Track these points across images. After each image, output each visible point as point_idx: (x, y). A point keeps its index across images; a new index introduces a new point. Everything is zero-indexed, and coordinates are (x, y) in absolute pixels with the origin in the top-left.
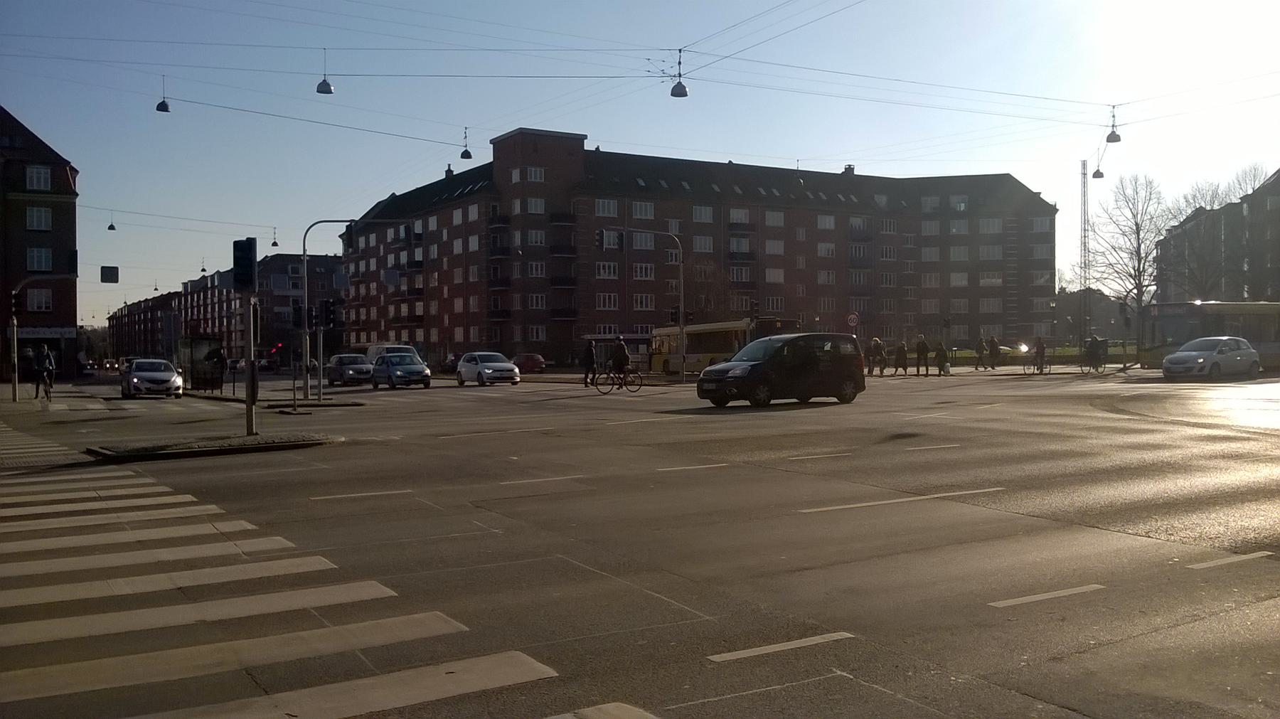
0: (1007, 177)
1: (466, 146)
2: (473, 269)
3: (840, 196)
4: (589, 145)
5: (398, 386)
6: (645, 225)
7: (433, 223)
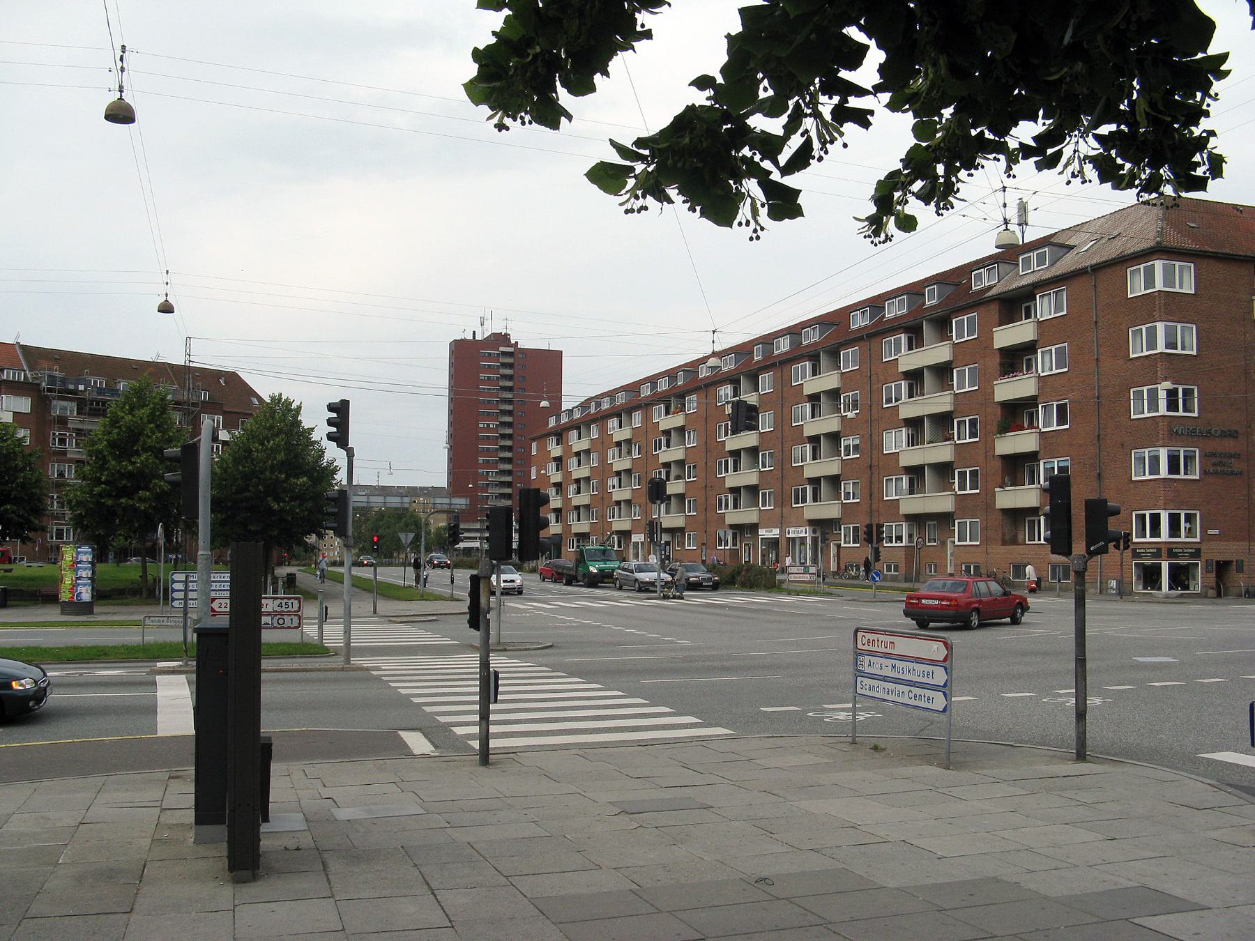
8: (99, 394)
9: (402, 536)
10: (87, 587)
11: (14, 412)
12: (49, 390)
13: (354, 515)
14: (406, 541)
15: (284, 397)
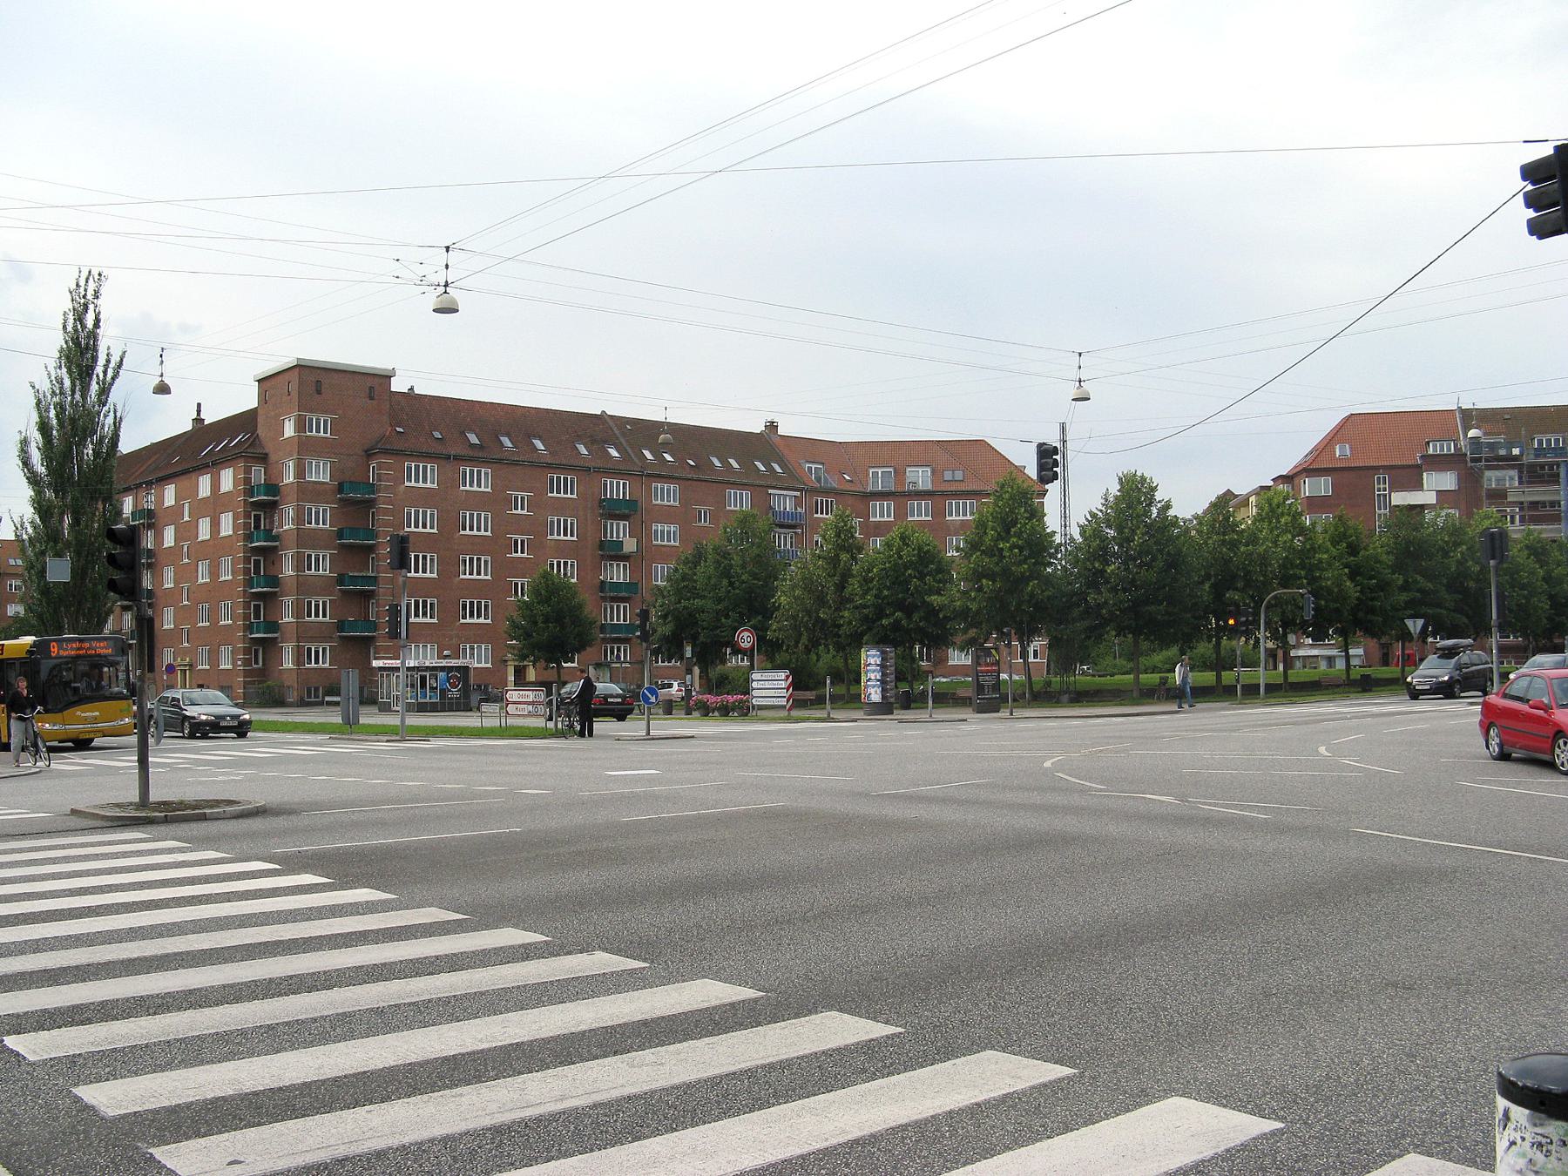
0: (981, 443)
1: (162, 376)
2: (226, 563)
3: (735, 465)
4: (398, 385)
5: (210, 735)
6: (479, 501)
7: (170, 495)
8: (1537, 456)
9: (1409, 623)
10: (875, 688)
11: (1437, 491)
12: (1474, 460)
13: (446, 657)
14: (1415, 630)
15: (1139, 474)
